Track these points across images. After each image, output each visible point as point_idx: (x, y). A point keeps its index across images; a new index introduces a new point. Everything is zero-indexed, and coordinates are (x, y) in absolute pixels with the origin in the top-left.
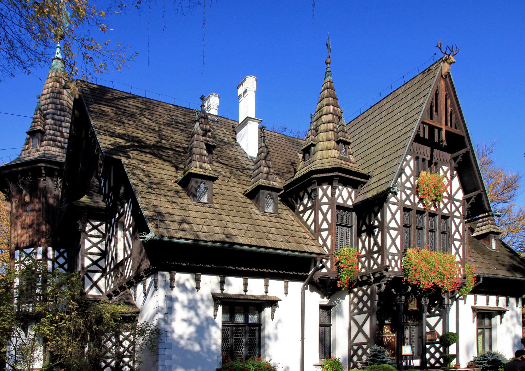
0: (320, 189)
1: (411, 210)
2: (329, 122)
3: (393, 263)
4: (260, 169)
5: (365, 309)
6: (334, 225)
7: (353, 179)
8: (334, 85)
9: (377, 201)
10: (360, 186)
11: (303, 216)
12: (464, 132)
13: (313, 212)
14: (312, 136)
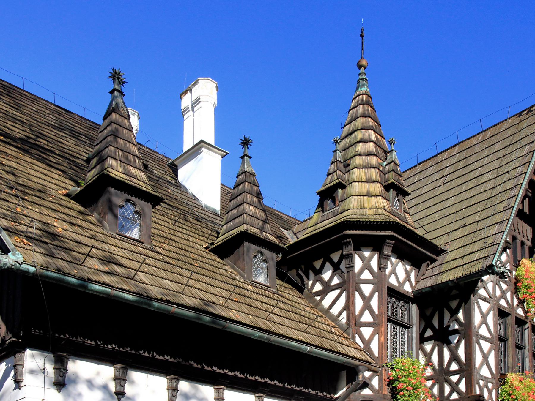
0: (357, 256)
1: (508, 315)
2: (370, 154)
4: (242, 207)
6: (385, 320)
8: (373, 102)
9: (455, 292)
10: (426, 264)
11: (321, 300)
13: (344, 294)
14: (339, 172)
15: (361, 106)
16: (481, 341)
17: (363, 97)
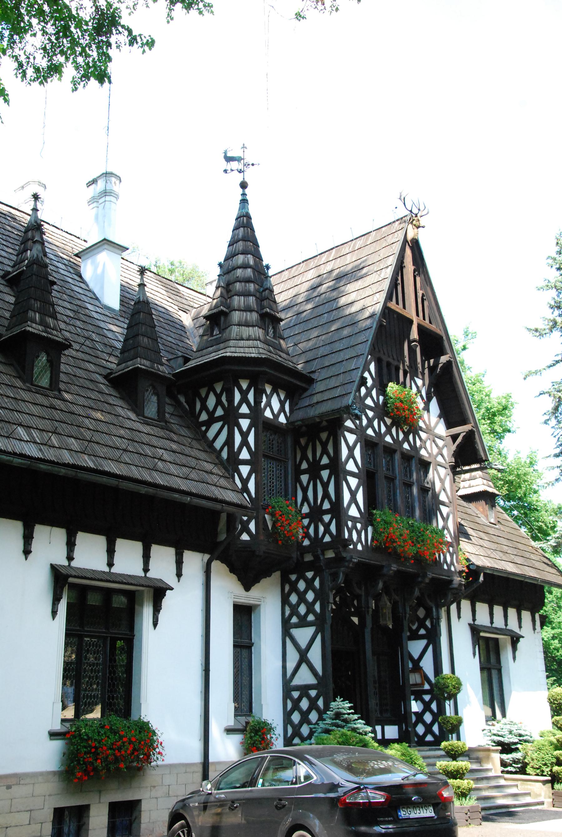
3: (355, 536)
5: (422, 632)
7: (295, 384)
11: (207, 430)
12: (441, 328)
15: (242, 229)
16: (349, 478)
17: (243, 219)
